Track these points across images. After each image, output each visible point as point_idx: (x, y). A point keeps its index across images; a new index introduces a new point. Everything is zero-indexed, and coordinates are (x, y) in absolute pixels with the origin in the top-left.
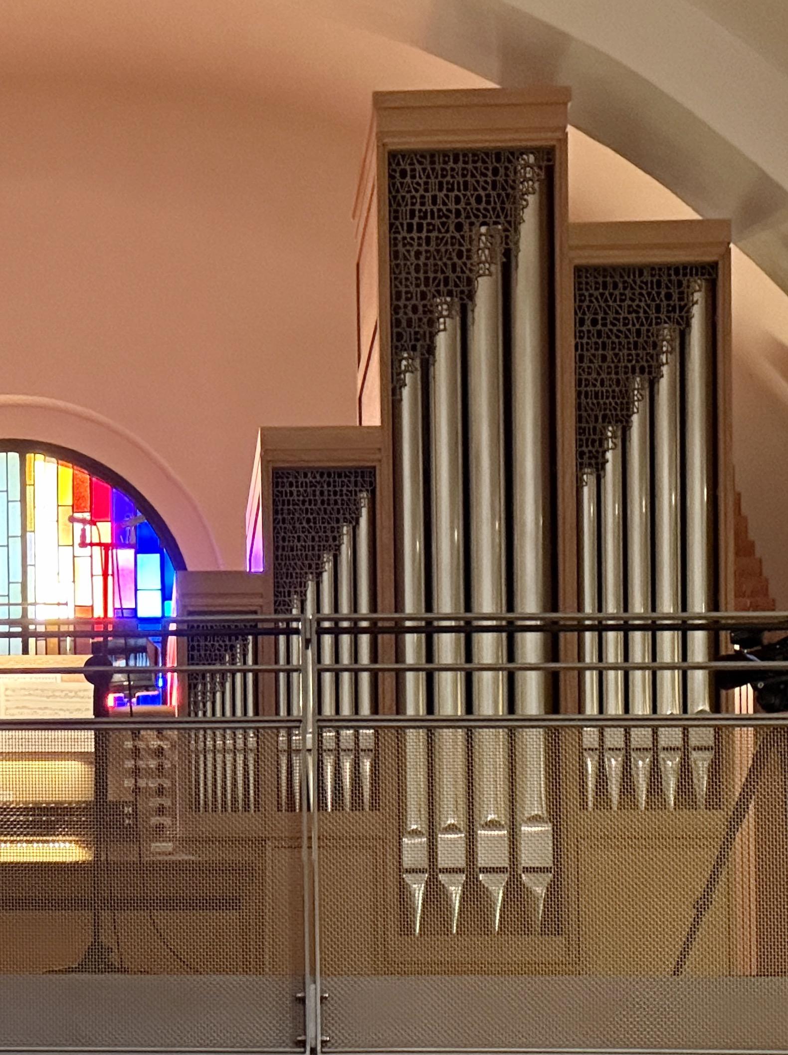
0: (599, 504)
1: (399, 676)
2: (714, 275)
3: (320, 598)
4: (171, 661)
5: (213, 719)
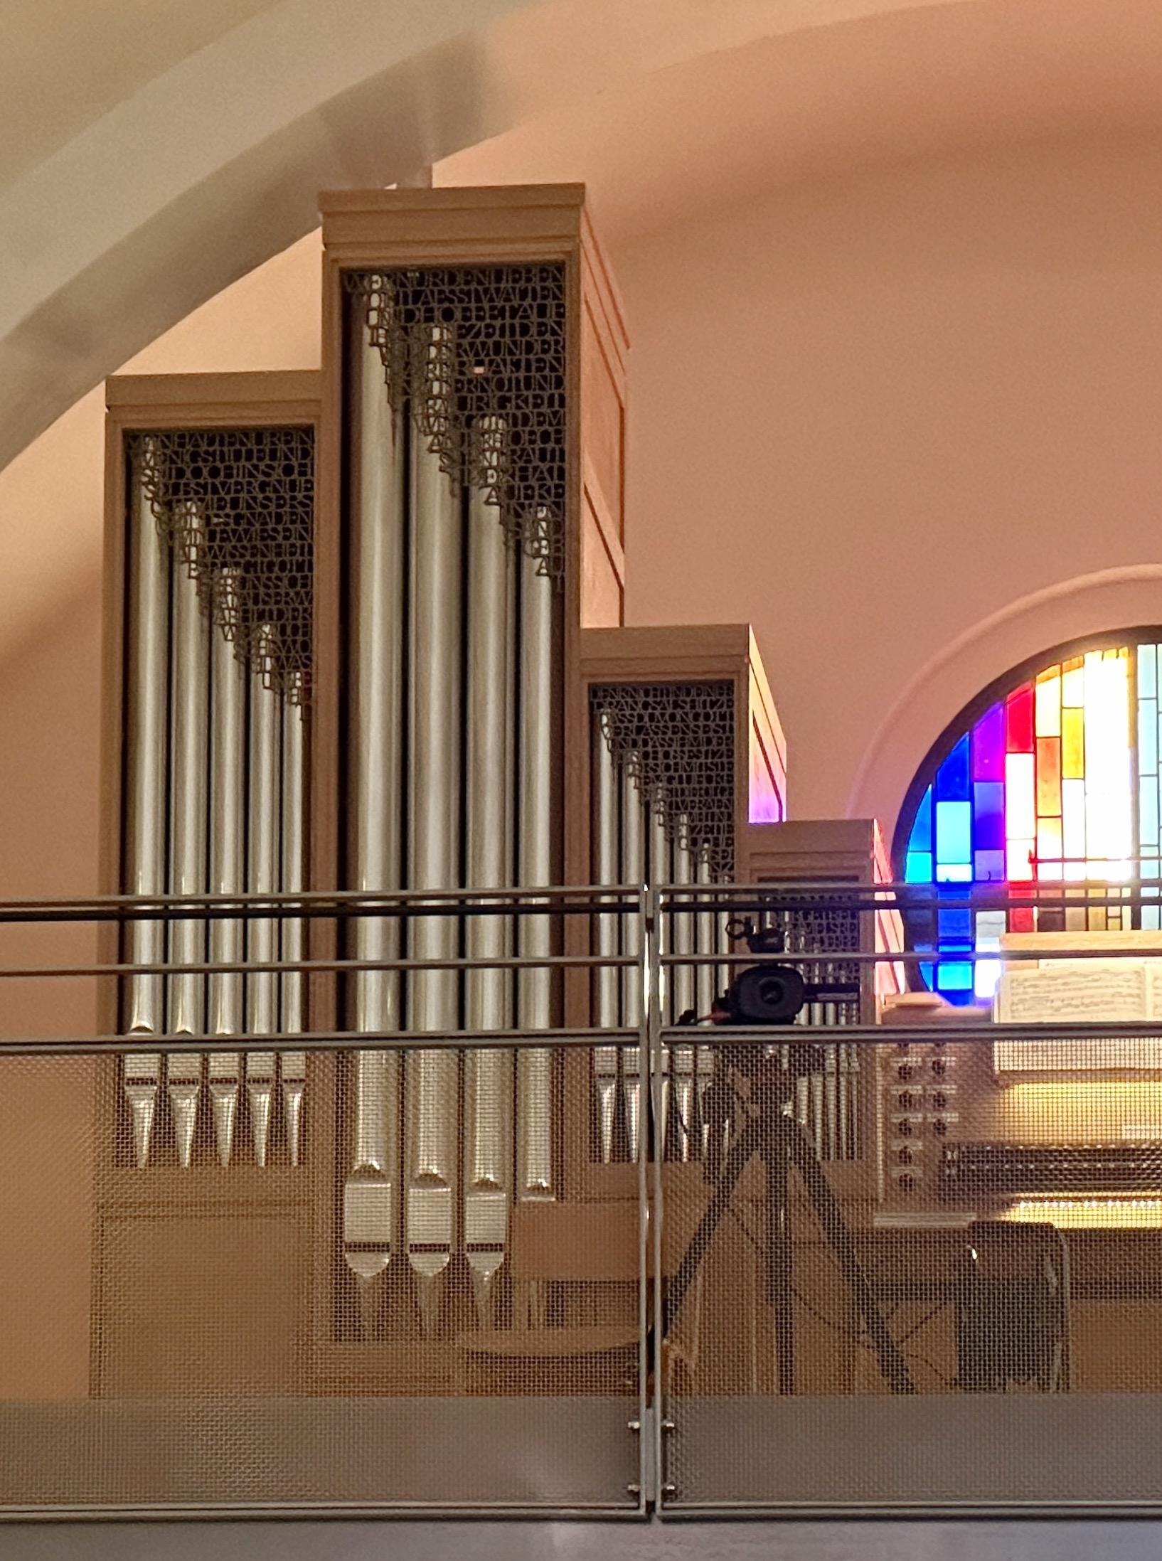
5: (823, 1028)
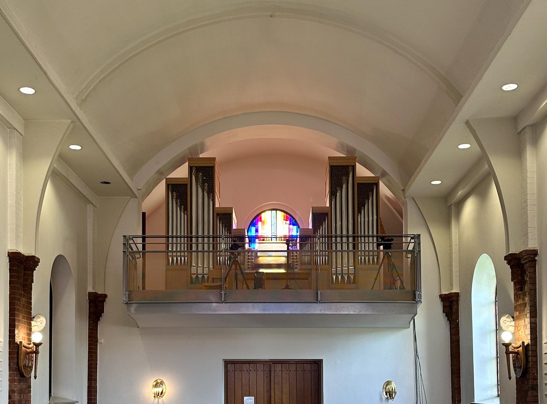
0: (361, 219)
1: (332, 244)
2: (377, 185)
3: (320, 232)
4: (298, 241)
